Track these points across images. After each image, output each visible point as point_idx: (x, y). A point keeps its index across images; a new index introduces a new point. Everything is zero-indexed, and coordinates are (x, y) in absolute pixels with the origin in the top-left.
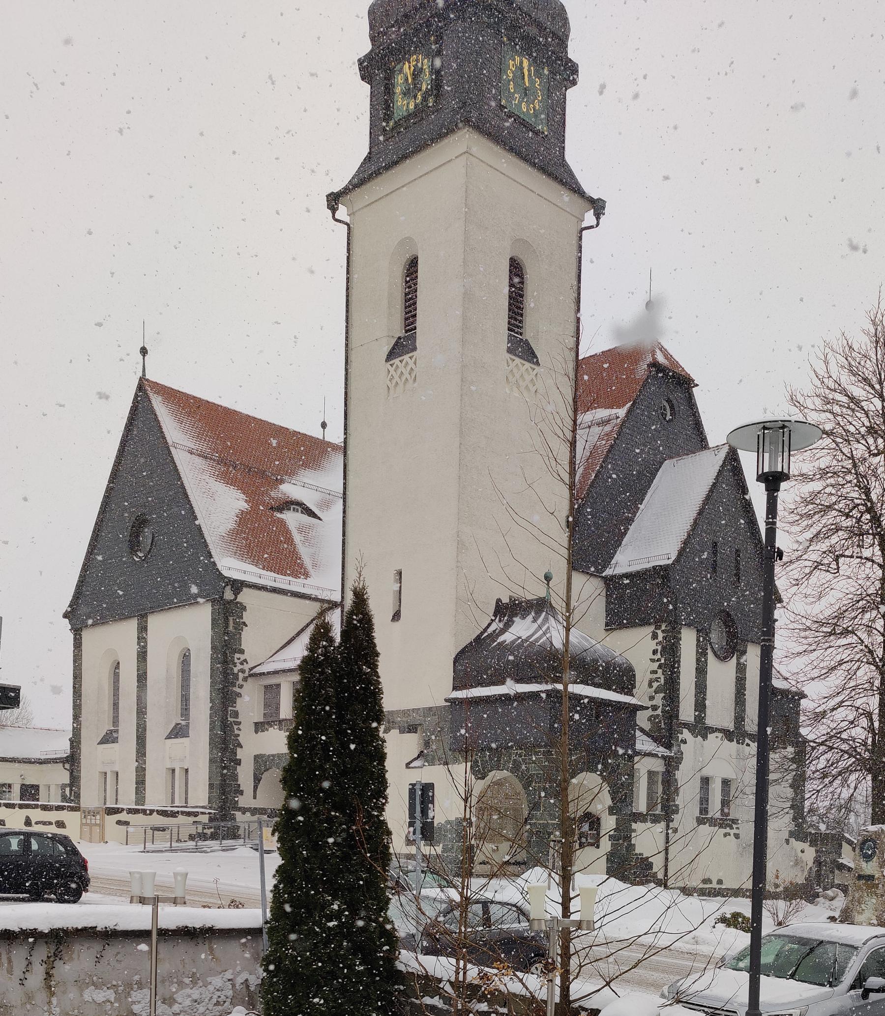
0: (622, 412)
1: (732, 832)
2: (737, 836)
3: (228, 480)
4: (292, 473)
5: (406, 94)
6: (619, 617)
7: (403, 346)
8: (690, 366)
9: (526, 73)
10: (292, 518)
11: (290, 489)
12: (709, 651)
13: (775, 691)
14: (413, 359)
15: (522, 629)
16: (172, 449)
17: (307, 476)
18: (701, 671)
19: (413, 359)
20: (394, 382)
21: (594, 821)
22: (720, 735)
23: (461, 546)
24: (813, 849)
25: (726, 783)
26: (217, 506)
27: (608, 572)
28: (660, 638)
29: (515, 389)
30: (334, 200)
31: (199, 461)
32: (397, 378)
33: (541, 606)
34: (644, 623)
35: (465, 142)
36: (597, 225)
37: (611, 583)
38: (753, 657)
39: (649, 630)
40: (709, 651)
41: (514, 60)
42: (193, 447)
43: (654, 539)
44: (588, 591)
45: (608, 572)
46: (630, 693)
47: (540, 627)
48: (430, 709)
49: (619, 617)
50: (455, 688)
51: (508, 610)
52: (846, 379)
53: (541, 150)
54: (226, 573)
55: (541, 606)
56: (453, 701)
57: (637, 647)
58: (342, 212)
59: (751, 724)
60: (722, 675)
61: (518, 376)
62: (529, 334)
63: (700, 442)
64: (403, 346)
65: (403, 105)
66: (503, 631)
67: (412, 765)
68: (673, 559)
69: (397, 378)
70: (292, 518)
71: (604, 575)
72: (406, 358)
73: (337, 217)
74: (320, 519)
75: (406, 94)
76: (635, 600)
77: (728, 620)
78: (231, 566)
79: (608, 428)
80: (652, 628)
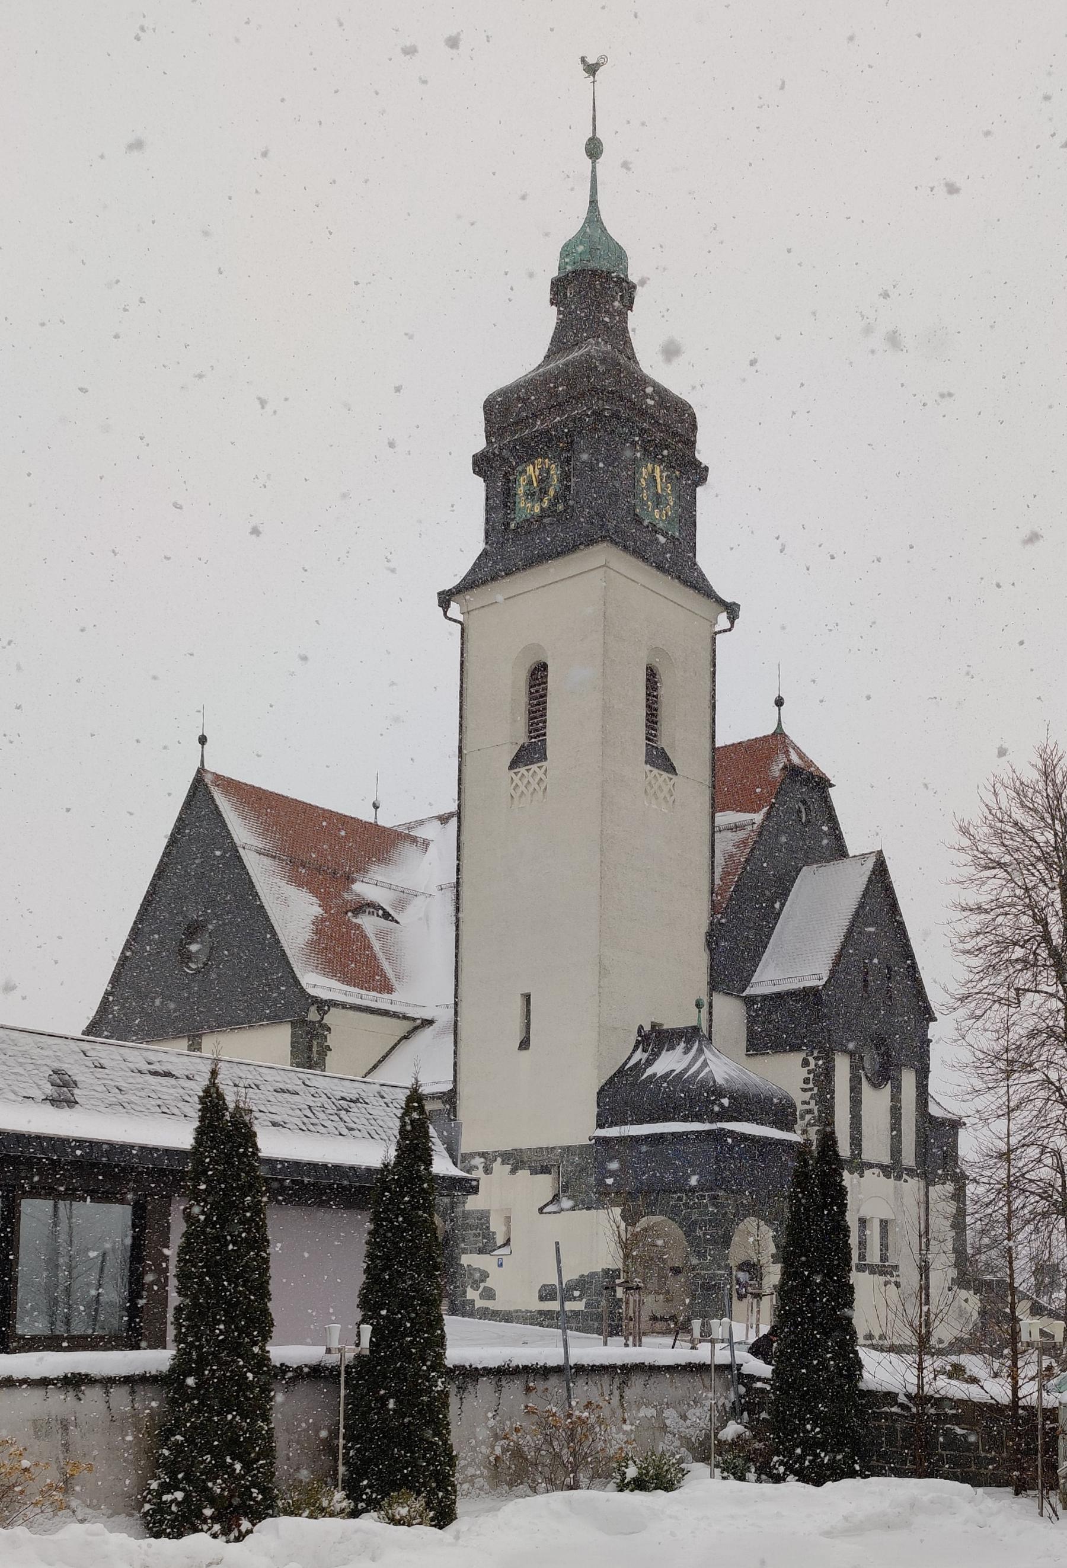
0: (758, 817)
1: (893, 1279)
2: (897, 1285)
3: (299, 882)
4: (363, 869)
5: (530, 495)
6: (760, 1042)
7: (530, 753)
8: (825, 765)
9: (658, 481)
10: (368, 923)
11: (364, 889)
12: (864, 1079)
13: (932, 1119)
14: (543, 769)
15: (670, 1062)
16: (240, 850)
17: (378, 872)
18: (856, 1102)
19: (543, 769)
20: (519, 791)
21: (752, 1268)
22: (876, 1171)
23: (603, 971)
24: (978, 1296)
25: (884, 1224)
26: (293, 913)
27: (749, 991)
28: (812, 1066)
29: (653, 801)
30: (445, 599)
31: (268, 861)
32: (522, 788)
33: (691, 1036)
34: (796, 1048)
35: (602, 555)
36: (732, 626)
37: (749, 1001)
38: (908, 1079)
39: (797, 1058)
40: (864, 1079)
41: (646, 468)
42: (261, 846)
43: (800, 954)
44: (729, 1013)
45: (749, 991)
46: (790, 1128)
47: (694, 1060)
48: (569, 1148)
49: (760, 1042)
50: (600, 1126)
51: (656, 1039)
52: (1018, 815)
53: (674, 557)
54: (311, 991)
55: (691, 1036)
56: (598, 1139)
57: (786, 1074)
58: (455, 610)
59: (909, 1158)
60: (876, 1102)
61: (656, 787)
62: (663, 742)
63: (839, 851)
64: (530, 753)
65: (527, 508)
66: (649, 1063)
67: (545, 1210)
68: (825, 979)
69: (522, 788)
70: (368, 923)
71: (744, 994)
72: (534, 767)
73: (459, 626)
74: (397, 922)
75: (530, 495)
76: (780, 1023)
77: (879, 1042)
78: (316, 982)
79: (741, 835)
80: (803, 1055)
